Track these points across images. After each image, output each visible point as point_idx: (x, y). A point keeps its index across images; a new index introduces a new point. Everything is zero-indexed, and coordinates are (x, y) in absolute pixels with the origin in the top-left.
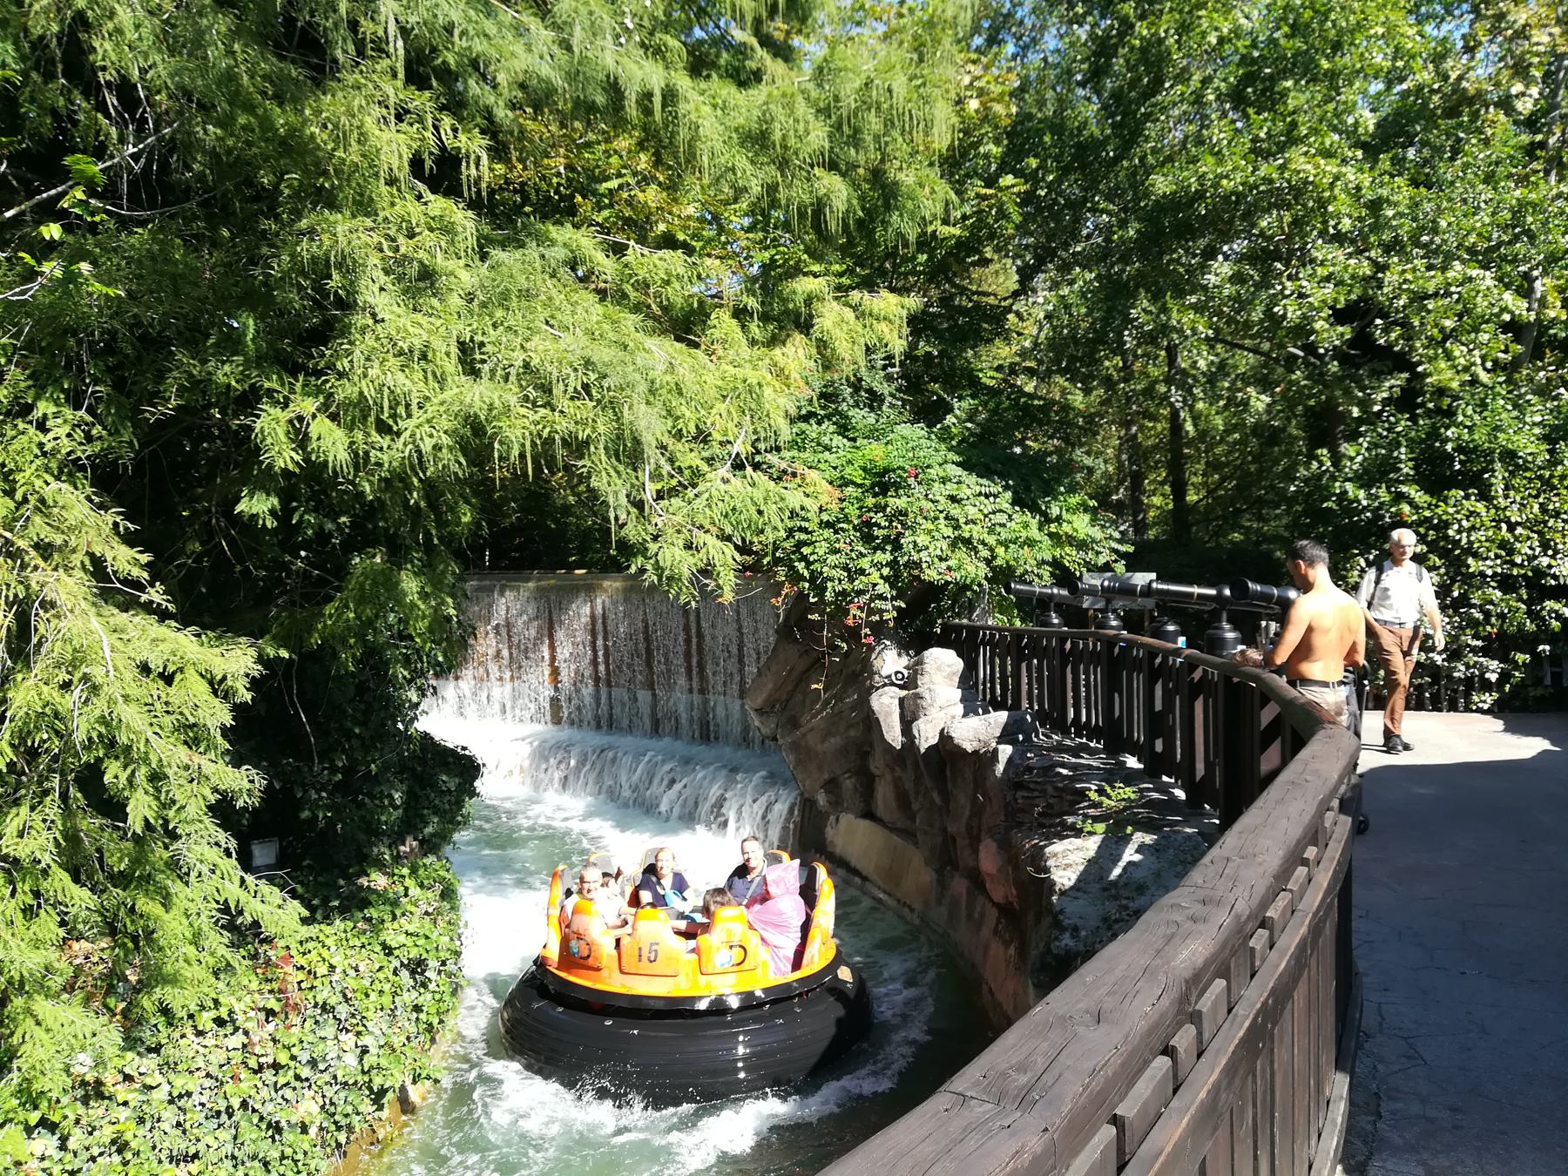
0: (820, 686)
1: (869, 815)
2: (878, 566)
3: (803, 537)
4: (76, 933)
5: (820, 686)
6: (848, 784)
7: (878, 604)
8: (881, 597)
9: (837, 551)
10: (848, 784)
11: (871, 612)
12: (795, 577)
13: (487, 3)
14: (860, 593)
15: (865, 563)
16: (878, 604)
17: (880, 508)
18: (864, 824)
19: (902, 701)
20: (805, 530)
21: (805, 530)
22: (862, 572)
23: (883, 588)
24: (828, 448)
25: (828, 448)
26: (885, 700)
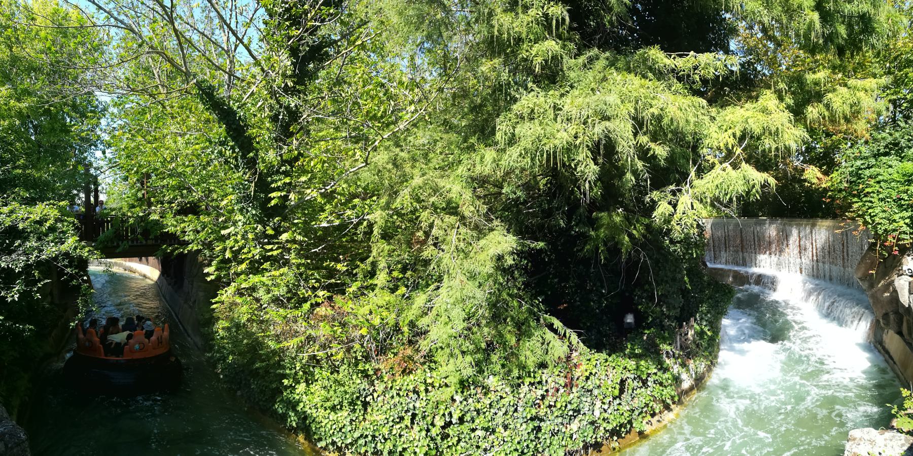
0: (874, 272)
1: (900, 333)
2: (903, 218)
3: (870, 204)
4: (430, 388)
5: (874, 272)
6: (892, 317)
7: (903, 236)
8: (905, 233)
9: (884, 211)
10: (892, 317)
11: (899, 240)
12: (866, 223)
13: (4, 181)
14: (894, 230)
15: (896, 217)
16: (903, 236)
17: (906, 192)
18: (897, 337)
19: (910, 283)
20: (871, 202)
21: (871, 202)
22: (894, 221)
23: (905, 228)
24: (890, 166)
25: (890, 166)
26: (902, 282)
